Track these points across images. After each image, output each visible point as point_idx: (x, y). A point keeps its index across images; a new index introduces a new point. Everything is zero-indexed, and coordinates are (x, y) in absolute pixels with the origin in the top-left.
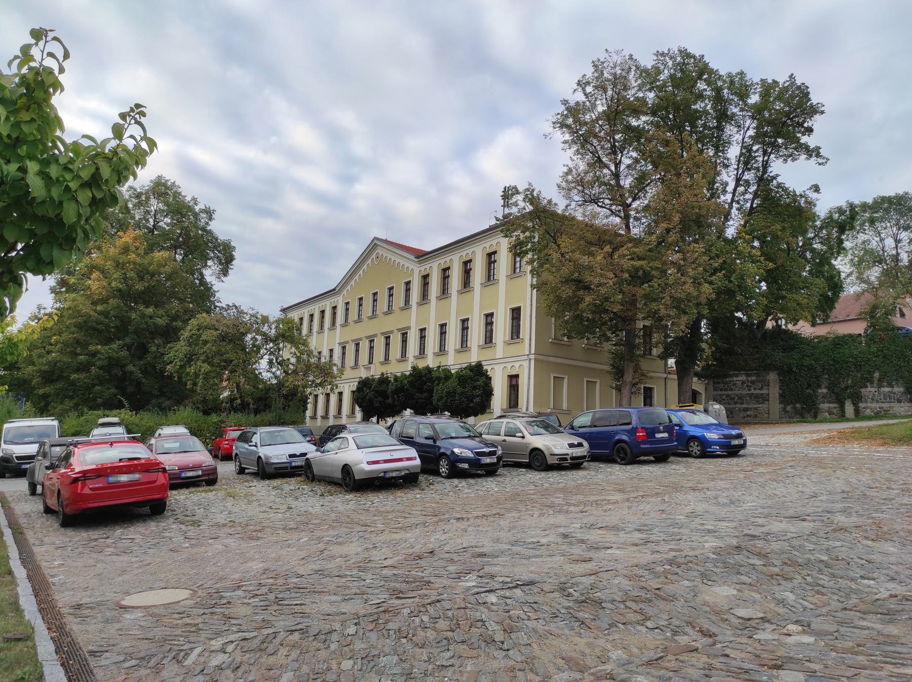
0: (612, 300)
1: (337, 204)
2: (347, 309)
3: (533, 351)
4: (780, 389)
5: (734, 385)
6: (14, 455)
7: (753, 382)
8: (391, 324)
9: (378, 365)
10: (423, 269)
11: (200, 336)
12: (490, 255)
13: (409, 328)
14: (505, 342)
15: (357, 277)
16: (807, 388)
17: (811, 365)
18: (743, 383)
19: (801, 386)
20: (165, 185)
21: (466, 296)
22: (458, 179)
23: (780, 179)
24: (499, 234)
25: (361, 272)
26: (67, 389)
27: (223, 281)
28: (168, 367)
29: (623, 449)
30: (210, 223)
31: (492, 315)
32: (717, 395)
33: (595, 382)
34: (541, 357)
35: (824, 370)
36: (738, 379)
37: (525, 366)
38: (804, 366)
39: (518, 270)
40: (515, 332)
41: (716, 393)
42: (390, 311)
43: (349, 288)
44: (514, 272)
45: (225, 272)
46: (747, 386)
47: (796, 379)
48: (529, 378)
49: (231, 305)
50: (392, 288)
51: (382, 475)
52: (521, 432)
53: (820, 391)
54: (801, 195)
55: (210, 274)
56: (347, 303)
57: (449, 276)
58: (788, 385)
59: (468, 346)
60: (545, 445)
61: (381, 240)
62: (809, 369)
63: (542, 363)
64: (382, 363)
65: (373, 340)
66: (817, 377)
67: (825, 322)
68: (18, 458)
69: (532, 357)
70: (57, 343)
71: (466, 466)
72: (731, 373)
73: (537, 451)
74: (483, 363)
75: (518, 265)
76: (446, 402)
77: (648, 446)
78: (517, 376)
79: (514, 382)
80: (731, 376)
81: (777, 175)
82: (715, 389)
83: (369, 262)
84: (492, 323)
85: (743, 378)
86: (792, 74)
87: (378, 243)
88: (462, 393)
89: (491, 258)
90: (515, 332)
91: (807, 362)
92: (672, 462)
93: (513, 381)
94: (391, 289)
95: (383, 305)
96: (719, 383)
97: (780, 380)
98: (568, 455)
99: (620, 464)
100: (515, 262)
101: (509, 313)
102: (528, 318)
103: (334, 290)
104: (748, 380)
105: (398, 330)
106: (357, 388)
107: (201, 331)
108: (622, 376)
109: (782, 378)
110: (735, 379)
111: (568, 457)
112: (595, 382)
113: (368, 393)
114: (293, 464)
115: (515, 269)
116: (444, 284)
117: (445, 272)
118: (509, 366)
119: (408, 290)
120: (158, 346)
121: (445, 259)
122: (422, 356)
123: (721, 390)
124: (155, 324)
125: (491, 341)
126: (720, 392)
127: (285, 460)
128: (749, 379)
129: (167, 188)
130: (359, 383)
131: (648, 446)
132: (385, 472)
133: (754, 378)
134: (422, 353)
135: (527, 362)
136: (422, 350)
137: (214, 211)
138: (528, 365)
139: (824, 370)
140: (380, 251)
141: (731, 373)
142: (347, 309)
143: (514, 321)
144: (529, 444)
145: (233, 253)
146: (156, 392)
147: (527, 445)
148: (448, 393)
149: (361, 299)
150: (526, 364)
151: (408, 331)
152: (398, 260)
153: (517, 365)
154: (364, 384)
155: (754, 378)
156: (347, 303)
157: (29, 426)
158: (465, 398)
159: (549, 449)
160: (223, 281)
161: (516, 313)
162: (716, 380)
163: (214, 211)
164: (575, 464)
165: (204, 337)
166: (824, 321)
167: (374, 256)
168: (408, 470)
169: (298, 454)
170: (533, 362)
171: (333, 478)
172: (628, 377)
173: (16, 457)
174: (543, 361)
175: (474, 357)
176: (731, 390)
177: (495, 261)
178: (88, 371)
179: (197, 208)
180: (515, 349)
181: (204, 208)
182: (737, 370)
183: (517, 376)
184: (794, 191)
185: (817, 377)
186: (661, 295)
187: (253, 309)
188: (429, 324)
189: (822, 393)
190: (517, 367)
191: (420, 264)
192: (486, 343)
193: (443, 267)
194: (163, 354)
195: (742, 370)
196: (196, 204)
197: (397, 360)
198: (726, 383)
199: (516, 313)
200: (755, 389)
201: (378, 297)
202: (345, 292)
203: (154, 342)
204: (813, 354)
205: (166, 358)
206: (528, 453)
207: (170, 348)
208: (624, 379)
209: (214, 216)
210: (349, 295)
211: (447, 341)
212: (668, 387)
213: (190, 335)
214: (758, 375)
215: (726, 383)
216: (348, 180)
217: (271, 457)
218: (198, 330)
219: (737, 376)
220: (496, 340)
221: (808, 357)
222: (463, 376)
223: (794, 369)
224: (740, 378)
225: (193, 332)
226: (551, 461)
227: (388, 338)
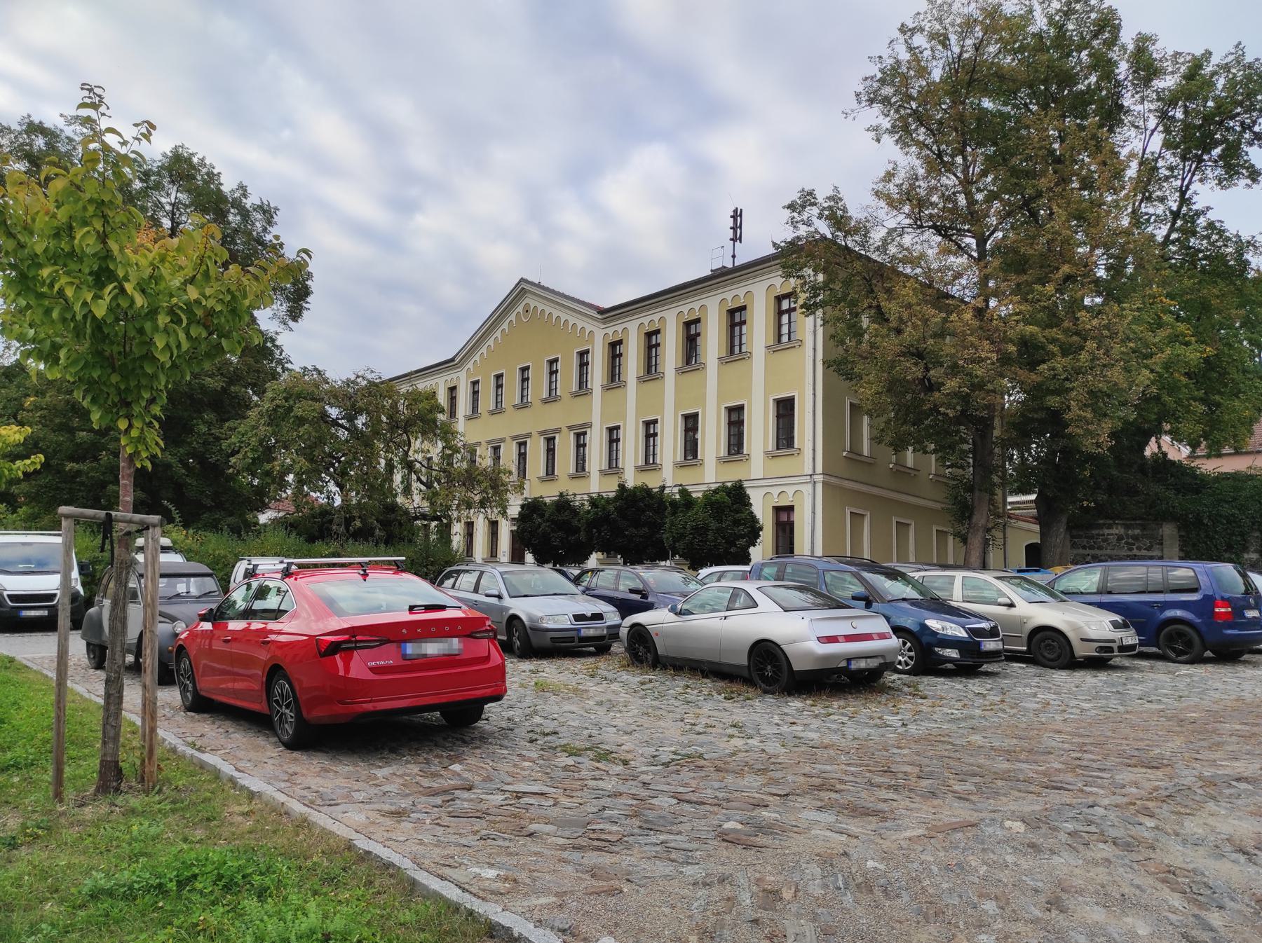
0: (990, 386)
1: (389, 242)
2: (475, 393)
3: (819, 469)
4: (1181, 550)
5: (1105, 540)
6: (5, 593)
7: (1136, 538)
8: (559, 417)
9: (536, 482)
10: (610, 331)
11: (290, 409)
12: (649, 335)
13: (589, 425)
14: (766, 453)
15: (491, 342)
16: (1226, 551)
17: (1233, 515)
18: (1120, 538)
19: (1215, 546)
20: (188, 160)
21: (651, 386)
22: (572, 218)
23: (1211, 215)
24: (776, 270)
25: (498, 334)
26: (58, 488)
27: (291, 330)
28: (233, 460)
29: (1181, 635)
30: (270, 229)
31: (740, 409)
32: (1077, 555)
33: (908, 525)
34: (833, 480)
35: (1253, 524)
36: (1111, 531)
37: (806, 493)
38: (1221, 516)
39: (785, 339)
40: (785, 437)
41: (1075, 552)
42: (498, 410)
43: (477, 357)
44: (779, 341)
45: (295, 313)
46: (1127, 543)
47: (1207, 536)
48: (814, 513)
49: (310, 368)
50: (501, 375)
51: (843, 664)
52: (1004, 595)
53: (1246, 556)
54: (1248, 242)
55: (267, 319)
56: (475, 383)
57: (621, 355)
58: (1194, 545)
59: (620, 465)
60: (1068, 623)
61: (532, 283)
62: (1229, 522)
63: (834, 491)
64: (542, 480)
65: (525, 443)
66: (1242, 535)
67: (1238, 452)
68: (12, 597)
69: (820, 478)
70: (37, 408)
71: (953, 653)
72: (1101, 522)
73: (1039, 636)
74: (746, 484)
75: (785, 330)
76: (692, 543)
77: (1236, 632)
78: (790, 509)
79: (784, 518)
80: (1101, 527)
81: (1208, 208)
82: (1074, 546)
83: (513, 317)
84: (741, 423)
85: (1118, 530)
86: (1240, 43)
87: (527, 287)
88: (718, 529)
89: (736, 318)
90: (785, 437)
91: (1226, 510)
92: (1245, 662)
93: (784, 515)
94: (499, 377)
95: (538, 386)
96: (1079, 537)
97: (1180, 536)
98: (1113, 641)
99: (1174, 662)
100: (780, 326)
101: (680, 422)
102: (809, 417)
103: (452, 360)
104: (1127, 535)
105: (570, 428)
106: (520, 514)
107: (291, 402)
108: (970, 517)
109: (1183, 533)
110: (1106, 531)
111: (1115, 646)
112: (908, 525)
113: (540, 525)
114: (584, 633)
115: (780, 335)
116: (613, 367)
117: (651, 341)
118: (775, 491)
119: (583, 365)
120: (210, 424)
121: (691, 306)
122: (550, 477)
123: (1084, 547)
124: (202, 387)
125: (695, 456)
126: (1081, 551)
127: (567, 625)
128: (1130, 532)
129: (192, 166)
130: (523, 506)
131: (1236, 632)
132: (849, 660)
133: (1137, 531)
134: (550, 473)
135: (810, 487)
136: (550, 469)
137: (277, 209)
138: (811, 491)
139: (1253, 524)
140: (531, 302)
141: (1101, 522)
142: (475, 393)
143: (781, 420)
144: (1029, 618)
145: (309, 283)
146: (208, 502)
147: (1022, 622)
148: (696, 529)
149: (499, 377)
150: (807, 489)
151: (588, 430)
152: (564, 317)
153: (790, 490)
154: (532, 509)
155: (1137, 531)
156: (475, 383)
157: (24, 544)
158: (723, 538)
159: (1077, 629)
160: (291, 330)
161: (785, 408)
162: (1075, 532)
163: (277, 209)
164: (1100, 661)
165: (298, 412)
166: (1235, 449)
167: (520, 309)
168: (883, 656)
169: (589, 615)
170: (819, 487)
171: (719, 664)
172: (980, 518)
173: (9, 596)
174: (834, 487)
175: (730, 475)
176: (1100, 548)
177: (658, 345)
178: (96, 459)
179: (248, 203)
180: (785, 465)
181: (259, 203)
182: (1111, 519)
183: (790, 509)
184: (1237, 236)
185: (1242, 535)
186: (1068, 385)
187: (372, 372)
188: (624, 418)
189: (1250, 559)
190: (791, 495)
191: (605, 323)
192: (729, 454)
193: (648, 329)
194: (218, 439)
195: (1119, 518)
196: (245, 196)
197: (539, 478)
198: (1092, 537)
199: (785, 408)
200: (1139, 549)
201: (480, 387)
202: (470, 365)
203: (202, 418)
204: (1235, 499)
205: (225, 444)
206: (1025, 635)
207: (230, 429)
208: (974, 520)
209: (276, 218)
210: (479, 368)
211: (620, 453)
212: (1009, 541)
213: (272, 406)
214: (1144, 528)
215: (1092, 537)
216: (405, 207)
217: (542, 618)
218: (286, 399)
219: (1110, 527)
220: (624, 463)
221: (1227, 502)
222: (717, 502)
223: (1205, 521)
224: (1115, 531)
225: (278, 402)
226: (1081, 651)
227: (522, 444)
